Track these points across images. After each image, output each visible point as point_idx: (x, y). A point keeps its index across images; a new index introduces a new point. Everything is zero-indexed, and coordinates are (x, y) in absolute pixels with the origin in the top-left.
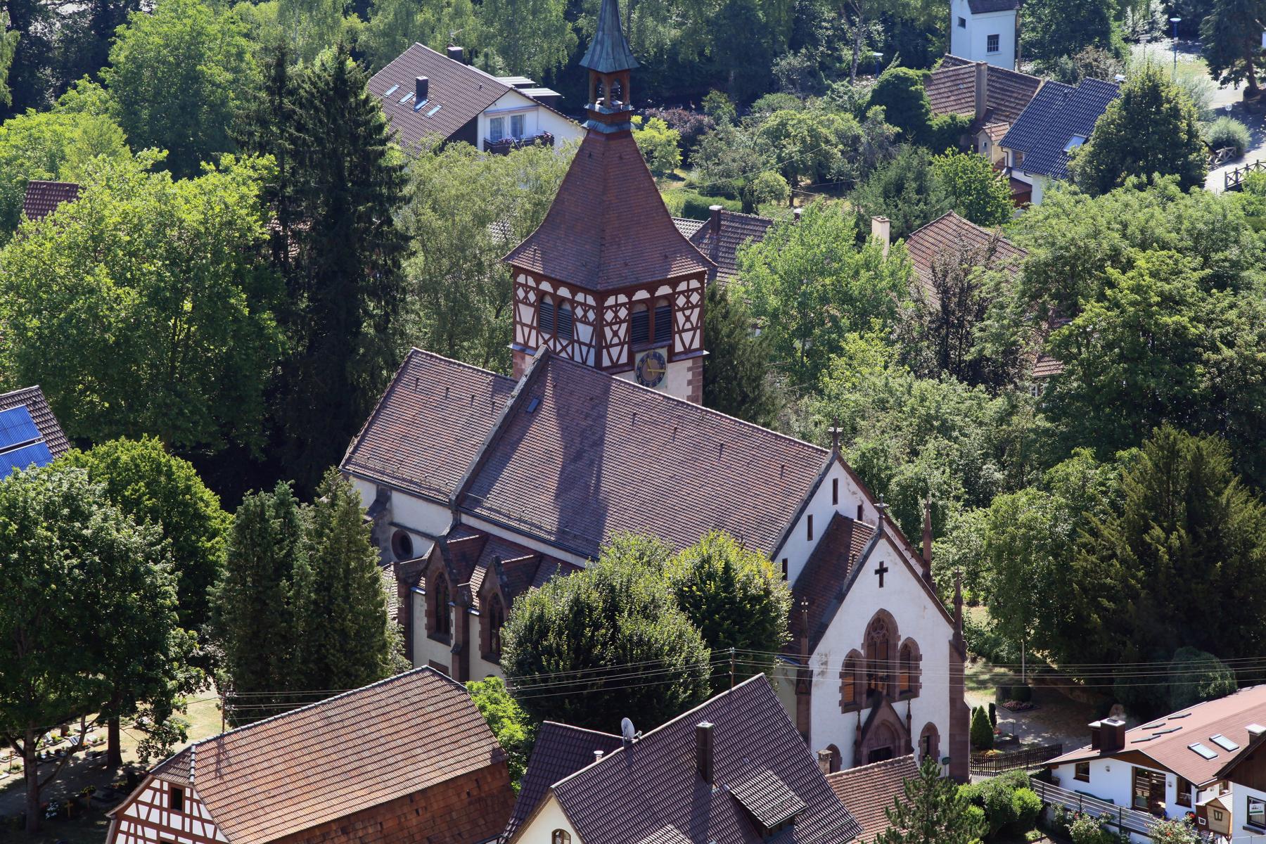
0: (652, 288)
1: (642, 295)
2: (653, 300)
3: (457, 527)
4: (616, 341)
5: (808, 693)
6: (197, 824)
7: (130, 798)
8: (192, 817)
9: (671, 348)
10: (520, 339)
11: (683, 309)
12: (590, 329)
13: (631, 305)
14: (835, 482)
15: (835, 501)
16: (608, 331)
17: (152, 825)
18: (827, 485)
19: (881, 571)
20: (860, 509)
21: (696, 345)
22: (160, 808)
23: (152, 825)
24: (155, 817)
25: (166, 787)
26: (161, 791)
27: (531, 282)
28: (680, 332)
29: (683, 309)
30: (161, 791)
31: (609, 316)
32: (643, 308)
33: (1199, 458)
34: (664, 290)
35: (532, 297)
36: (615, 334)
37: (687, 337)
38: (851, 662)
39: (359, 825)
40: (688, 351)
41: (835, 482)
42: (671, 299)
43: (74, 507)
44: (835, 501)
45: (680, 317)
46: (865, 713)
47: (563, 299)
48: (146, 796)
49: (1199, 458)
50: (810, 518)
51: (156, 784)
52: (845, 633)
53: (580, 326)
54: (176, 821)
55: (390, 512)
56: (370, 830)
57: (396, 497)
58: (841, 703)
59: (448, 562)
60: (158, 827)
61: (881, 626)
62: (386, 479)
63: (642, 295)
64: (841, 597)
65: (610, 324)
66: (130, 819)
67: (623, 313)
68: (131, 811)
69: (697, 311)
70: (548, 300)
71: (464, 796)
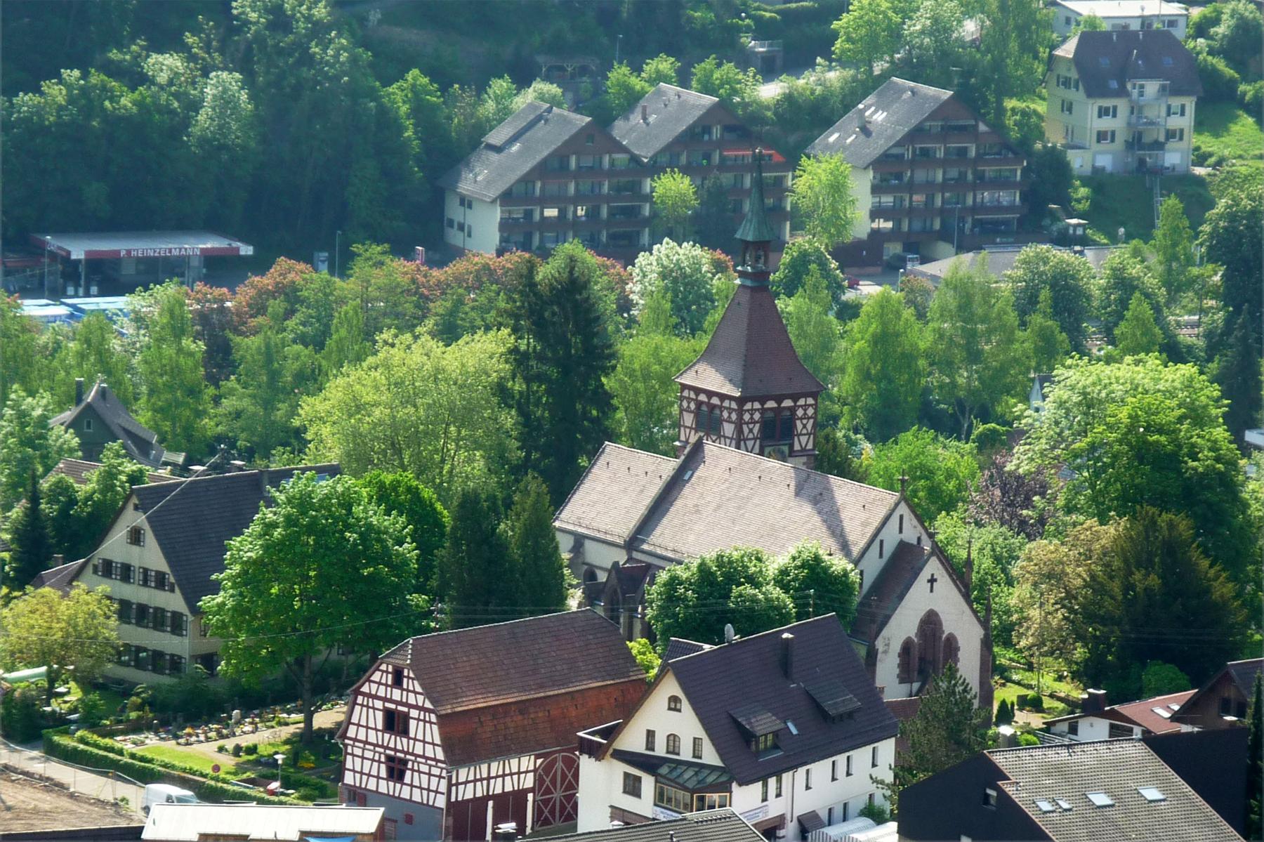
0: (779, 400)
1: (771, 404)
2: (778, 410)
3: (630, 559)
4: (751, 436)
5: (875, 665)
6: (411, 695)
7: (364, 678)
8: (408, 691)
9: (791, 446)
10: (683, 438)
11: (801, 419)
12: (733, 426)
13: (763, 411)
14: (901, 517)
15: (901, 531)
16: (745, 427)
17: (379, 698)
18: (895, 520)
19: (932, 581)
20: (919, 539)
21: (810, 446)
22: (386, 685)
23: (379, 698)
24: (381, 693)
25: (390, 669)
26: (387, 672)
27: (693, 395)
28: (798, 435)
29: (801, 419)
30: (387, 672)
31: (747, 417)
32: (770, 415)
33: (1171, 526)
34: (788, 403)
35: (693, 406)
36: (751, 431)
37: (804, 439)
38: (907, 648)
39: (532, 710)
40: (803, 450)
41: (901, 517)
42: (792, 410)
43: (347, 503)
44: (901, 531)
45: (799, 425)
46: (916, 686)
47: (714, 406)
48: (376, 676)
49: (1171, 526)
50: (882, 542)
51: (383, 667)
52: (903, 625)
53: (725, 424)
54: (397, 694)
55: (583, 554)
56: (540, 715)
57: (588, 543)
58: (898, 676)
59: (619, 579)
60: (385, 699)
61: (930, 622)
62: (580, 530)
63: (771, 404)
64: (901, 598)
65: (747, 423)
66: (364, 694)
67: (757, 416)
68: (365, 689)
69: (811, 421)
70: (704, 408)
71: (612, 701)
